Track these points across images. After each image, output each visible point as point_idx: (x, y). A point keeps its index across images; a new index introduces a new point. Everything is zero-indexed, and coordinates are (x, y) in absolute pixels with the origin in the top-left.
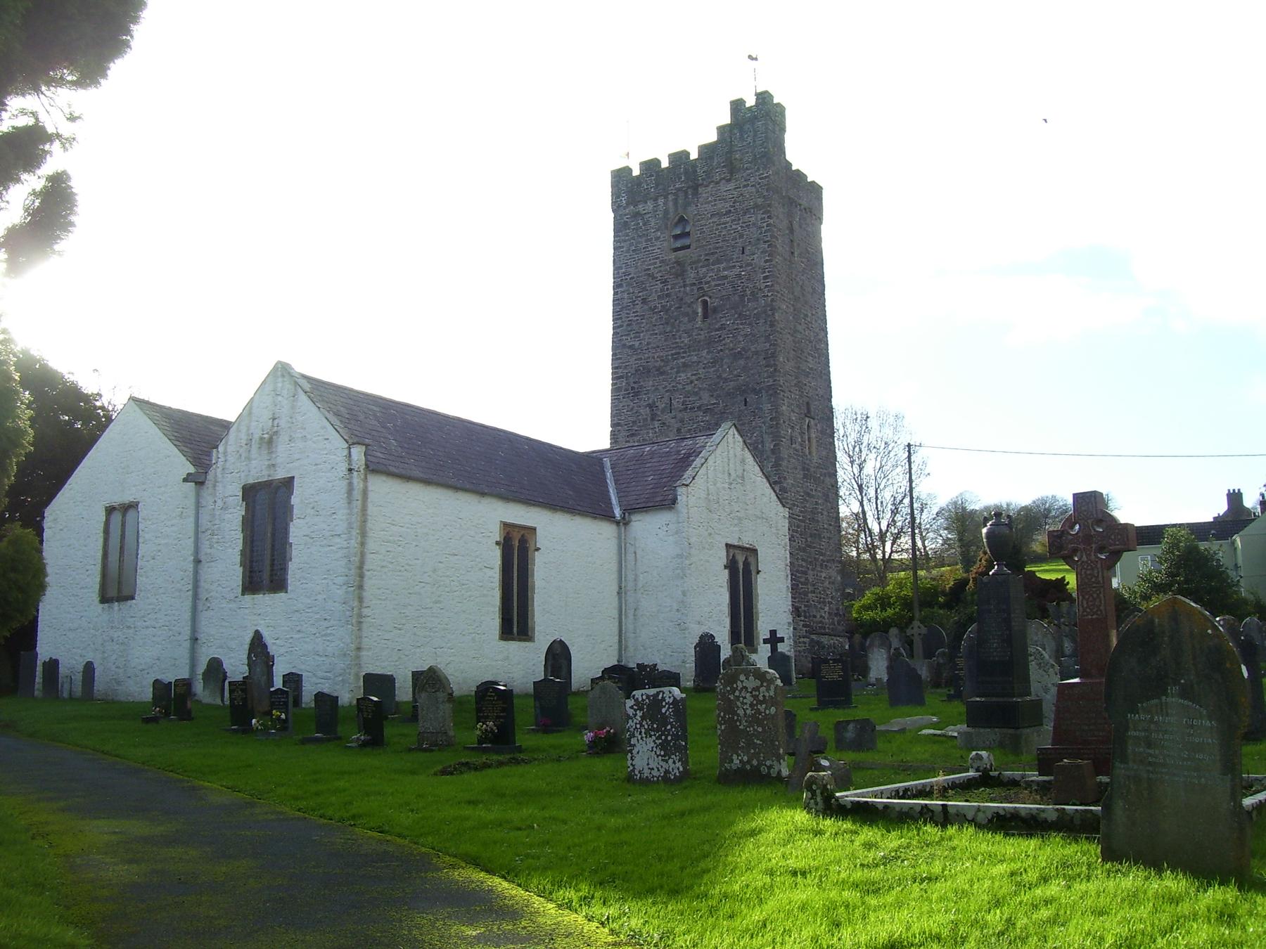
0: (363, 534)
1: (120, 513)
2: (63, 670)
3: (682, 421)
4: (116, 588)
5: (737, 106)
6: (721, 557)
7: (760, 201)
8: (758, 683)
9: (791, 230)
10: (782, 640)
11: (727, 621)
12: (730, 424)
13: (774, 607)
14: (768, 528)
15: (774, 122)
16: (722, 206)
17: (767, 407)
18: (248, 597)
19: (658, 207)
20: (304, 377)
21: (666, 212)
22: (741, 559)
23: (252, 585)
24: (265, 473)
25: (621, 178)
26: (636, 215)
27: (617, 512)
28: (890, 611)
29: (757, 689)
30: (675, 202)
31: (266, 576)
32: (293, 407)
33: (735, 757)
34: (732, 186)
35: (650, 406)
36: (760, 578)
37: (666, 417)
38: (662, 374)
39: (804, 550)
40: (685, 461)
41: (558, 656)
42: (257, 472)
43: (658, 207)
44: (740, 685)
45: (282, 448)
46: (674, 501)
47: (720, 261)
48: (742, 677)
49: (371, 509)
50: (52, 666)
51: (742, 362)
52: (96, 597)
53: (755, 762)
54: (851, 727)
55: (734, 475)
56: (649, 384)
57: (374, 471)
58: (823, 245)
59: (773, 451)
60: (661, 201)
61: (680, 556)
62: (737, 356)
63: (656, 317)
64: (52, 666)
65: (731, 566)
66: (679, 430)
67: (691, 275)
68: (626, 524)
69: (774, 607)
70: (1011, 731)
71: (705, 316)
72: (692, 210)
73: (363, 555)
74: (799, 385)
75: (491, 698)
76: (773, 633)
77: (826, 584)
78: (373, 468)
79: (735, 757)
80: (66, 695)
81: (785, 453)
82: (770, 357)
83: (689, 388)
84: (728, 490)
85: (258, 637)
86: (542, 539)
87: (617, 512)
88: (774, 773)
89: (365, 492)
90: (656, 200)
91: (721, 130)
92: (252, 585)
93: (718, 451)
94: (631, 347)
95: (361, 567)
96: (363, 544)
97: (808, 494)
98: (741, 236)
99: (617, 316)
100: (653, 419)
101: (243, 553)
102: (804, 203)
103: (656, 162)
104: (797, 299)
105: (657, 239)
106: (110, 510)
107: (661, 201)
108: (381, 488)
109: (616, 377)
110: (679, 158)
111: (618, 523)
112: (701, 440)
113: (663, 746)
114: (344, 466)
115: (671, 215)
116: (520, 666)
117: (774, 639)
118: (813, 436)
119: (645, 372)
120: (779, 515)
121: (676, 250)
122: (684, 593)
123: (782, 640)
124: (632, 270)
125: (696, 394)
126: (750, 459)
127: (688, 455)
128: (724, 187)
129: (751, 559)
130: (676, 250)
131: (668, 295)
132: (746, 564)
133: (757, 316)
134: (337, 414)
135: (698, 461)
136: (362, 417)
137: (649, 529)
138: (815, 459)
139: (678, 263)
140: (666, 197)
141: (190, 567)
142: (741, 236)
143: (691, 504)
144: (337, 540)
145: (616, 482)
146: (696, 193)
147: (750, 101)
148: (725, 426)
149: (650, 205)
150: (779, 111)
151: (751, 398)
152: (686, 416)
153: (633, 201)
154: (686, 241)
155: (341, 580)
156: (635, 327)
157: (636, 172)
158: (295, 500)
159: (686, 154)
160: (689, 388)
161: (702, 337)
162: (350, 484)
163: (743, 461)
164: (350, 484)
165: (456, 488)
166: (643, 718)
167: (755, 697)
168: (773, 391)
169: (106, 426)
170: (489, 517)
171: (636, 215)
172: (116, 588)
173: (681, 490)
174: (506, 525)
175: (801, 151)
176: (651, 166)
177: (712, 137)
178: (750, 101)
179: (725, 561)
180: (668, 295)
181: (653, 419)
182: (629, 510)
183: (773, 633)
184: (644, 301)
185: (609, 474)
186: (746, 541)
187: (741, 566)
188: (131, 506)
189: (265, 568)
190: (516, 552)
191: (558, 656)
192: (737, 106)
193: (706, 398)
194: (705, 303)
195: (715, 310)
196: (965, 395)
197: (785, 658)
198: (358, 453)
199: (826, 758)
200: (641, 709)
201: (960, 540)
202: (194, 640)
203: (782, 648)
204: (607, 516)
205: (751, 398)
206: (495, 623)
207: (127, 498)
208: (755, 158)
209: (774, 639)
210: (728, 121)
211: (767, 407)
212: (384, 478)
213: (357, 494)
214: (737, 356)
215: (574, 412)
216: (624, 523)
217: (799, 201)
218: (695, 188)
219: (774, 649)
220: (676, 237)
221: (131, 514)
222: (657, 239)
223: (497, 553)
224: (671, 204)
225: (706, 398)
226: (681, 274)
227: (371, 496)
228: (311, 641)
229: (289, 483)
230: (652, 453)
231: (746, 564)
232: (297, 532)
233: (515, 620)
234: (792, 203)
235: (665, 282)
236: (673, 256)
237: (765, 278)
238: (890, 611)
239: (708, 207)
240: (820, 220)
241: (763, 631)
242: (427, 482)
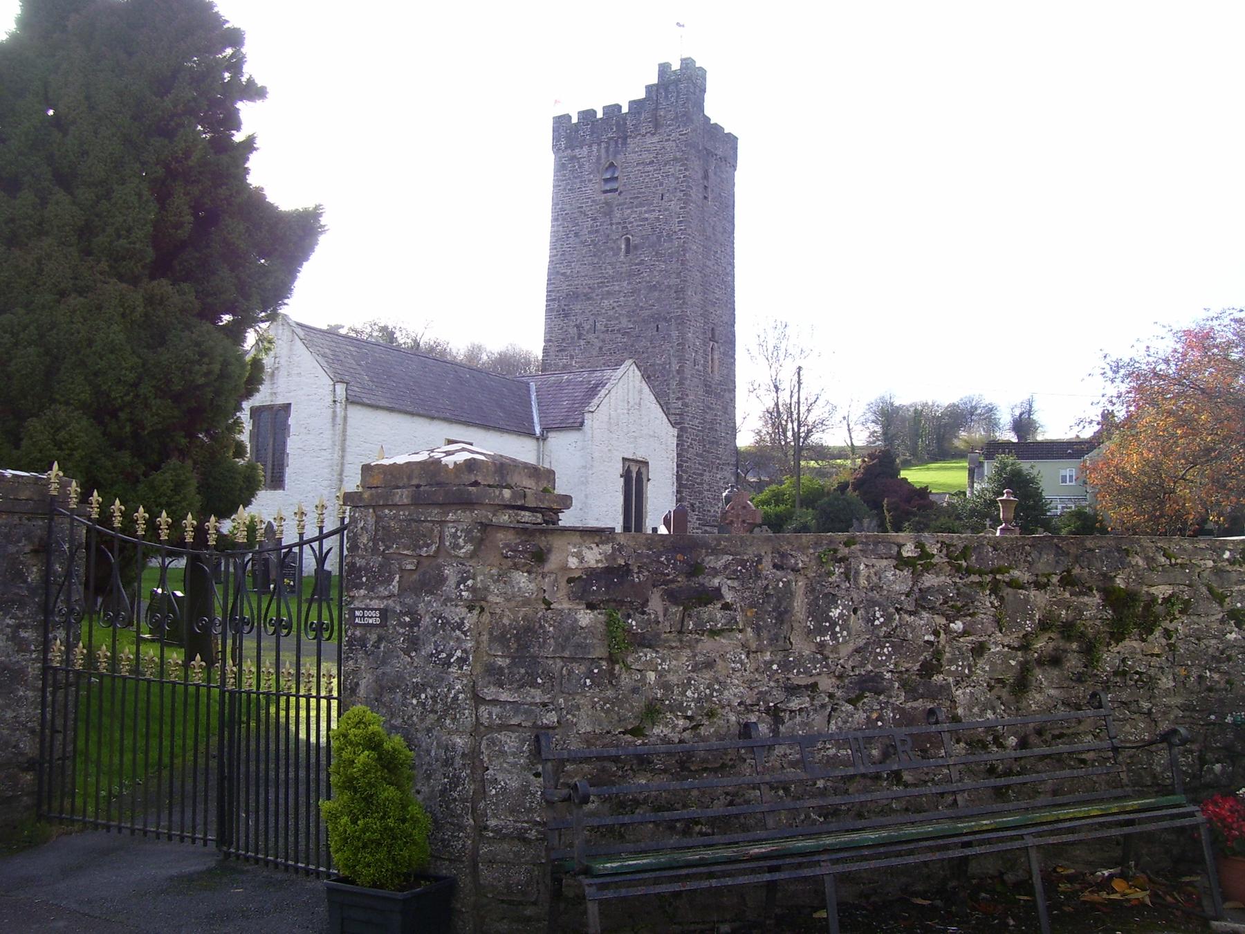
0: (343, 450)
3: (603, 341)
5: (664, 69)
6: (619, 468)
7: (678, 155)
9: (706, 177)
11: (621, 518)
12: (631, 361)
15: (695, 85)
16: (648, 157)
17: (675, 334)
19: (592, 145)
21: (599, 158)
22: (634, 469)
24: (268, 398)
25: (561, 123)
26: (573, 158)
27: (538, 430)
28: (782, 507)
30: (607, 149)
32: (291, 350)
34: (655, 139)
35: (577, 326)
36: (650, 485)
37: (591, 337)
38: (589, 299)
39: (701, 456)
40: (593, 391)
43: (592, 145)
46: (582, 424)
47: (647, 195)
49: (349, 431)
51: (656, 294)
55: (632, 403)
56: (577, 307)
57: (353, 403)
58: (736, 189)
59: (678, 372)
60: (595, 148)
61: (584, 467)
62: (653, 288)
63: (586, 249)
65: (627, 475)
66: (601, 348)
67: (617, 214)
68: (544, 440)
71: (628, 252)
72: (621, 157)
73: (342, 464)
74: (705, 315)
76: (108, 831)
77: (721, 484)
78: (351, 401)
81: (688, 373)
82: (680, 291)
83: (611, 313)
87: (538, 430)
89: (345, 418)
90: (590, 146)
91: (649, 88)
93: (620, 384)
94: (563, 274)
95: (341, 474)
96: (343, 457)
97: (709, 408)
98: (661, 184)
99: (553, 247)
100: (579, 338)
102: (719, 153)
104: (708, 238)
105: (590, 181)
107: (595, 148)
108: (358, 416)
109: (550, 300)
110: (612, 111)
111: (538, 439)
112: (608, 373)
114: (331, 399)
115: (603, 161)
118: (716, 357)
119: (574, 296)
120: (669, 435)
121: (605, 192)
122: (586, 496)
124: (567, 207)
125: (617, 318)
126: (646, 389)
127: (597, 385)
128: (649, 140)
129: (643, 470)
130: (605, 192)
131: (597, 231)
132: (639, 473)
133: (671, 256)
134: (324, 356)
135: (603, 392)
136: (342, 358)
138: (717, 377)
139: (606, 203)
140: (599, 145)
142: (661, 184)
143: (595, 426)
144: (323, 453)
145: (539, 404)
146: (625, 143)
147: (676, 66)
148: (628, 362)
149: (585, 149)
150: (702, 73)
151: (662, 325)
152: (607, 337)
153: (570, 146)
154: (614, 185)
155: (326, 483)
156: (568, 257)
157: (575, 120)
158: (291, 421)
159: (619, 107)
160: (611, 313)
161: (624, 270)
162: (334, 412)
163: (640, 392)
164: (334, 412)
165: (412, 414)
168: (682, 321)
169: (827, 925)
171: (573, 158)
173: (587, 416)
175: (718, 108)
176: (588, 115)
177: (642, 95)
178: (676, 66)
179: (621, 471)
180: (597, 231)
181: (579, 338)
182: (547, 429)
183: (108, 831)
184: (576, 235)
185: (533, 397)
187: (634, 475)
192: (664, 69)
193: (624, 322)
194: (628, 240)
195: (636, 247)
198: (340, 389)
201: (885, 434)
204: (531, 434)
205: (662, 325)
208: (676, 117)
210: (655, 81)
211: (675, 334)
212: (359, 407)
213: (339, 420)
214: (653, 288)
216: (543, 438)
217: (717, 151)
218: (625, 138)
220: (606, 181)
222: (590, 181)
224: (603, 151)
225: (624, 322)
226: (609, 214)
227: (349, 420)
229: (287, 407)
230: (569, 381)
231: (639, 473)
232: (292, 445)
235: (594, 219)
236: (603, 197)
237: (680, 222)
238: (782, 507)
239: (635, 156)
240: (734, 167)
242: (391, 410)
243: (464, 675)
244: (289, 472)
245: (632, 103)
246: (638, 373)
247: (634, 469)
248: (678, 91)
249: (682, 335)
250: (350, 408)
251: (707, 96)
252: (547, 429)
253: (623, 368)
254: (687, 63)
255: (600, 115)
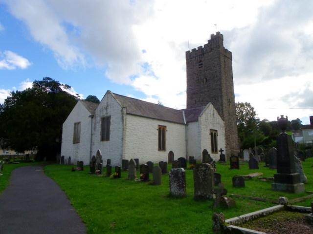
1: (77, 125)
2: (65, 158)
4: (76, 140)
6: (209, 132)
8: (205, 169)
10: (223, 151)
13: (221, 144)
14: (219, 125)
18: (102, 142)
20: (114, 93)
22: (214, 132)
23: (103, 139)
25: (188, 53)
27: (185, 123)
29: (205, 170)
31: (105, 137)
33: (199, 192)
41: (171, 154)
42: (104, 114)
44: (200, 169)
45: (109, 110)
47: (209, 67)
48: (201, 166)
50: (63, 157)
52: (72, 142)
53: (205, 193)
54: (237, 179)
64: (63, 157)
65: (211, 134)
69: (221, 144)
70: (289, 185)
71: (206, 81)
75: (162, 164)
76: (221, 149)
79: (199, 192)
80: (65, 163)
81: (224, 110)
84: (210, 117)
85: (98, 151)
86: (168, 129)
88: (211, 197)
92: (103, 139)
101: (101, 133)
103: (195, 49)
106: (75, 124)
110: (200, 48)
111: (185, 125)
113: (179, 186)
116: (164, 157)
117: (221, 151)
120: (222, 123)
121: (200, 67)
123: (223, 151)
126: (215, 111)
128: (210, 53)
130: (200, 67)
132: (215, 133)
137: (193, 126)
138: (231, 111)
141: (90, 136)
147: (215, 34)
148: (210, 103)
157: (191, 52)
159: (202, 47)
166: (174, 177)
167: (205, 173)
168: (221, 96)
170: (157, 123)
172: (76, 140)
174: (159, 126)
176: (194, 50)
177: (207, 43)
178: (215, 34)
183: (221, 149)
186: (215, 129)
188: (79, 123)
189: (105, 136)
190: (162, 131)
191: (171, 154)
196: (265, 95)
197: (224, 155)
199: (226, 197)
200: (173, 174)
202: (91, 152)
203: (224, 153)
204: (183, 124)
205: (216, 98)
206: (157, 147)
207: (78, 121)
209: (221, 151)
215: (178, 101)
216: (187, 125)
218: (203, 54)
219: (221, 153)
220: (200, 65)
221: (79, 125)
223: (210, 136)
228: (110, 153)
233: (162, 146)
234: (225, 56)
240: (231, 60)
241: (219, 149)
243: (15, 101)
244: (111, 136)
245: (205, 45)
246: (212, 106)
247: (214, 132)
248: (217, 40)
249: (222, 101)
250: (130, 120)
251: (224, 42)
252: (188, 122)
253: (208, 105)
254: (218, 33)
255: (197, 49)
